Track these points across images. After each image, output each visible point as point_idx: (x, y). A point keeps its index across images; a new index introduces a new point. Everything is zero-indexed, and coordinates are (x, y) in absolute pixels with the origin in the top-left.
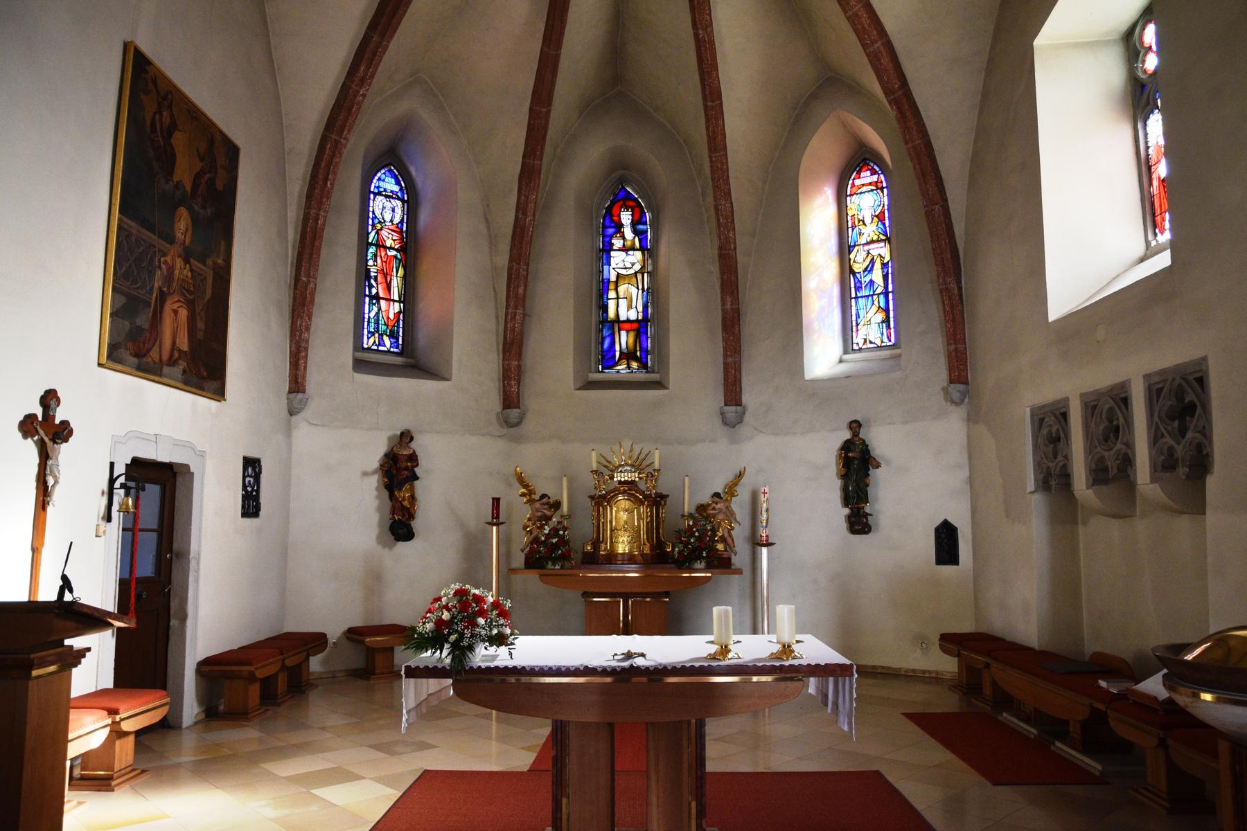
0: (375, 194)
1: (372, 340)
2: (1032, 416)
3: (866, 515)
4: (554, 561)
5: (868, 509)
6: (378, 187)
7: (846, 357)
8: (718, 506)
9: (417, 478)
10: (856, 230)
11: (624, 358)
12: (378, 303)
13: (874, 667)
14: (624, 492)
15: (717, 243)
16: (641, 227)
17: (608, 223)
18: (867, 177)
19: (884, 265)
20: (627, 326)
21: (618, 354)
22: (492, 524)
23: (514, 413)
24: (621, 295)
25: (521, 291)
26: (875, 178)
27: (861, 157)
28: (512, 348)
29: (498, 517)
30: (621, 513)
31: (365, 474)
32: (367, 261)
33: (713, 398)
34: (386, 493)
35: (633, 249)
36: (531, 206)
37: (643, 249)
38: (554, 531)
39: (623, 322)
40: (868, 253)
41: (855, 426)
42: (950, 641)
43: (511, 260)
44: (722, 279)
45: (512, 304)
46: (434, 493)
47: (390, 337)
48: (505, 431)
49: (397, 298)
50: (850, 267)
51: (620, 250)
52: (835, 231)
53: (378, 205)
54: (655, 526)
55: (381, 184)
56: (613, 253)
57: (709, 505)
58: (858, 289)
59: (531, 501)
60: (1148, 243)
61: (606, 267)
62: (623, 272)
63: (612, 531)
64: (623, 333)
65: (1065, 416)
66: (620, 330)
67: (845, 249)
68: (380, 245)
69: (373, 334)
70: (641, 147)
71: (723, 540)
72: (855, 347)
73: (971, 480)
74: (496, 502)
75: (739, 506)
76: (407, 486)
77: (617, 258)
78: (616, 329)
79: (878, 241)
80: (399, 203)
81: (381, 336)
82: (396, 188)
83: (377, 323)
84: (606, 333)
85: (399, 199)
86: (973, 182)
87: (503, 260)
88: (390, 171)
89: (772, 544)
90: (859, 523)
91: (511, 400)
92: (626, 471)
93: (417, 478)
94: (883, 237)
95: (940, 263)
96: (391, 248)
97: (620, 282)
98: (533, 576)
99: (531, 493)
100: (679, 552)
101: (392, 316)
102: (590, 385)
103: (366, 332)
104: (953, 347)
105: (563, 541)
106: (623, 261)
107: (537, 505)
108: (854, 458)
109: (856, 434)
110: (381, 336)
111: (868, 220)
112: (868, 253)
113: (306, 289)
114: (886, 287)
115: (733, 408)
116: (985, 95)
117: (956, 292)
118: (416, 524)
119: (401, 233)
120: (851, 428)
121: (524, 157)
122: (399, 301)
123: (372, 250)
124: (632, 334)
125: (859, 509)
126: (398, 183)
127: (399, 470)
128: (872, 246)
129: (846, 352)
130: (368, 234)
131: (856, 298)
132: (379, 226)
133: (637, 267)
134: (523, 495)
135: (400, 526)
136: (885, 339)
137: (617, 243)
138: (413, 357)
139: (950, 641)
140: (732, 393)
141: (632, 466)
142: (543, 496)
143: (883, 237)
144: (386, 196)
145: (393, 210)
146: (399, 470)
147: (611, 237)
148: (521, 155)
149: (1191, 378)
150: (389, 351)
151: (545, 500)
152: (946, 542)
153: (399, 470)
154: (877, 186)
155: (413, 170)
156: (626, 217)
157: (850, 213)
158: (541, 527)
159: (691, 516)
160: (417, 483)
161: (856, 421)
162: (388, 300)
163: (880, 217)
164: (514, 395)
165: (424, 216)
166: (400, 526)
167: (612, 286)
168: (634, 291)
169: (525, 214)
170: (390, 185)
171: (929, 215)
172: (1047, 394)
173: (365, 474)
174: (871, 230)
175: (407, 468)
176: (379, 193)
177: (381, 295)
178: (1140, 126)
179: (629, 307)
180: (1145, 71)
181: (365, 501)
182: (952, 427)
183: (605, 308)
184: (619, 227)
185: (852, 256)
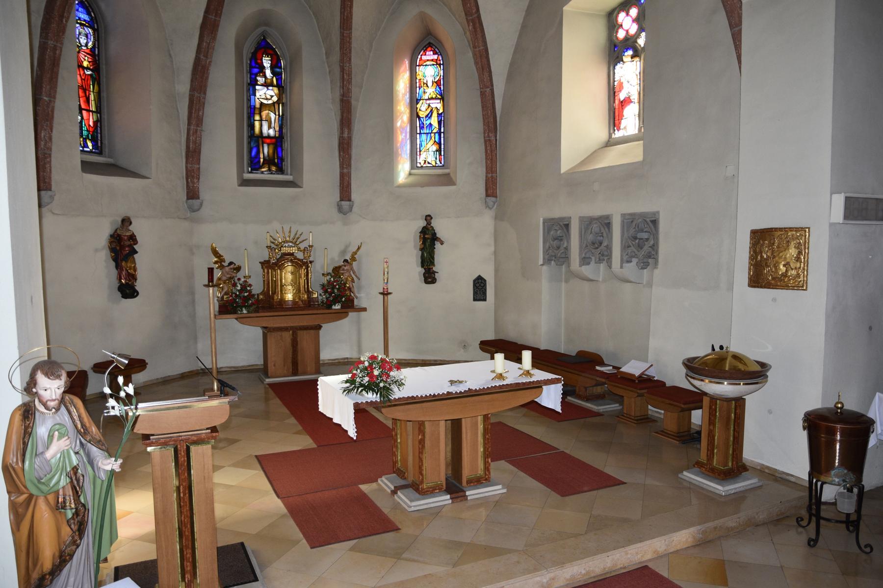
2: (544, 223)
3: (434, 272)
5: (434, 269)
7: (414, 171)
9: (136, 252)
10: (422, 89)
11: (269, 159)
16: (278, 70)
17: (253, 65)
18: (430, 55)
19: (439, 115)
20: (268, 141)
21: (262, 160)
22: (208, 286)
23: (195, 202)
24: (264, 117)
27: (428, 41)
29: (212, 281)
31: (96, 250)
33: (418, 271)
34: (113, 264)
35: (272, 85)
37: (279, 86)
39: (266, 137)
41: (428, 218)
43: (192, 89)
45: (194, 122)
46: (145, 262)
47: (92, 141)
51: (262, 85)
52: (416, 84)
56: (257, 87)
58: (422, 128)
60: (610, 135)
61: (252, 97)
62: (265, 102)
65: (567, 226)
66: (263, 143)
67: (414, 101)
72: (419, 165)
73: (495, 253)
79: (436, 99)
81: (85, 140)
82: (86, 17)
84: (253, 144)
86: (510, 77)
90: (430, 277)
91: (192, 194)
93: (136, 252)
95: (486, 123)
96: (87, 68)
101: (91, 124)
102: (245, 183)
104: (490, 175)
106: (264, 94)
107: (227, 269)
109: (429, 223)
110: (85, 140)
111: (430, 84)
114: (440, 129)
115: (348, 203)
116: (524, 26)
118: (138, 286)
121: (207, 12)
122: (96, 112)
124: (271, 147)
126: (88, 14)
129: (412, 168)
131: (420, 133)
133: (275, 99)
137: (261, 80)
141: (295, 243)
142: (231, 263)
145: (87, 37)
146: (122, 247)
147: (256, 75)
148: (203, 10)
149: (648, 220)
150: (91, 152)
152: (479, 288)
153: (122, 247)
154: (437, 63)
156: (267, 62)
157: (418, 77)
160: (136, 256)
161: (429, 216)
162: (88, 111)
163: (438, 83)
165: (114, 46)
167: (257, 111)
168: (272, 116)
171: (482, 94)
172: (558, 212)
173: (96, 250)
174: (431, 91)
177: (83, 106)
178: (612, 68)
179: (270, 127)
180: (617, 38)
183: (252, 126)
184: (262, 68)
185: (418, 106)
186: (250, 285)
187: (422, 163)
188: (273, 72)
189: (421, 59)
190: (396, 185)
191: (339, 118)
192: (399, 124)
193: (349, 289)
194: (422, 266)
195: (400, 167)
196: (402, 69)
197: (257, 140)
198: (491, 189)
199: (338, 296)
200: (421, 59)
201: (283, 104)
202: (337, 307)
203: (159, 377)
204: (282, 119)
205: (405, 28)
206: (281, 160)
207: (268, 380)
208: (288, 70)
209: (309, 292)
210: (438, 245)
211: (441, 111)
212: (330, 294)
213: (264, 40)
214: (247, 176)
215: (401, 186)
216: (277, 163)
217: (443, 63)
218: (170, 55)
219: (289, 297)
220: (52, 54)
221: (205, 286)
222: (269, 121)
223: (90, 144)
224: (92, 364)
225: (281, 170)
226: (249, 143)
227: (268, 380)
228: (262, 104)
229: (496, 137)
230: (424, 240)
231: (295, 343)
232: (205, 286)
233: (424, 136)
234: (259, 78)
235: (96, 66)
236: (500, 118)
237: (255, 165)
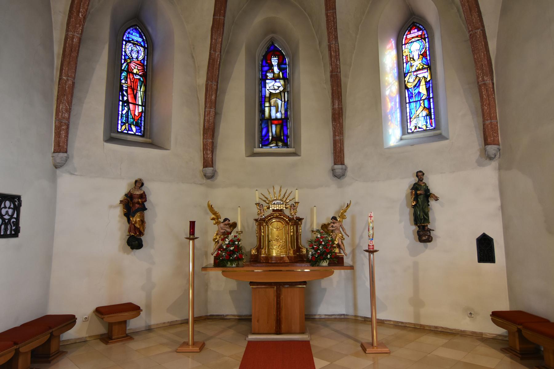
0: (126, 42)
1: (124, 127)
3: (429, 230)
4: (232, 261)
5: (429, 226)
6: (128, 38)
7: (404, 137)
8: (334, 225)
9: (146, 209)
11: (274, 135)
12: (128, 106)
13: (436, 327)
14: (277, 217)
15: (329, 69)
16: (283, 66)
17: (264, 64)
18: (415, 33)
19: (427, 83)
20: (276, 122)
21: (270, 138)
23: (209, 170)
25: (213, 97)
26: (420, 33)
27: (412, 22)
28: (210, 131)
30: (276, 229)
31: (111, 207)
32: (121, 80)
33: (327, 161)
35: (279, 78)
36: (219, 46)
37: (284, 78)
38: (232, 241)
39: (274, 119)
40: (417, 76)
42: (498, 317)
43: (208, 79)
44: (333, 90)
45: (208, 105)
47: (136, 126)
48: (205, 181)
49: (140, 103)
50: (406, 85)
51: (271, 79)
53: (128, 48)
54: (296, 239)
55: (130, 36)
56: (267, 81)
57: (329, 224)
58: (410, 97)
59: (218, 223)
61: (263, 89)
62: (273, 92)
63: (269, 241)
64: (274, 127)
66: (272, 124)
67: (402, 75)
68: (129, 71)
69: (124, 124)
70: (284, 18)
71: (339, 246)
72: (409, 131)
73: (503, 208)
74: (192, 224)
75: (346, 223)
76: (138, 214)
77: (270, 84)
78: (270, 124)
79: (423, 69)
80: (142, 49)
81: (130, 125)
82: (140, 40)
83: (127, 117)
84: (263, 126)
85: (141, 46)
87: (202, 80)
88: (136, 29)
89: (376, 251)
90: (424, 234)
91: (208, 162)
92: (278, 204)
93: (146, 209)
94: (425, 66)
97: (272, 97)
98: (216, 274)
99: (218, 217)
100: (312, 255)
101: (137, 114)
103: (120, 122)
105: (238, 248)
106: (273, 86)
107: (222, 225)
108: (421, 194)
109: (421, 180)
110: (130, 125)
111: (416, 57)
112: (417, 76)
113: (66, 85)
115: (340, 166)
117: (491, 86)
119: (143, 65)
120: (417, 176)
121: (214, 16)
122: (142, 106)
123: (124, 74)
124: (279, 127)
125: (424, 227)
126: (141, 37)
127: (134, 204)
128: (418, 72)
129: (403, 133)
130: (122, 64)
131: (410, 102)
132: (129, 61)
133: (281, 89)
134: (213, 219)
135: (135, 241)
136: (429, 126)
137: (270, 75)
138: (147, 133)
139: (498, 317)
140: (338, 156)
142: (226, 220)
143: (425, 66)
144: (134, 44)
145: (138, 52)
146: (134, 204)
147: (266, 72)
150: (135, 135)
151: (226, 222)
152: (485, 249)
153: (134, 204)
154: (422, 37)
155: (150, 29)
156: (275, 61)
157: (405, 54)
158: (223, 240)
159: (318, 231)
161: (421, 172)
162: (135, 104)
163: (424, 55)
164: (210, 160)
165: (157, 56)
166: (135, 241)
167: (267, 100)
168: (279, 102)
169: (215, 51)
170: (136, 37)
173: (111, 207)
174: (418, 63)
175: (138, 203)
176: (129, 42)
177: (130, 101)
179: (277, 111)
181: (116, 224)
182: (489, 173)
183: (262, 112)
184: (271, 66)
185: (406, 79)
186: (239, 240)
187: (413, 129)
188: (280, 69)
189: (406, 38)
190: (385, 147)
191: (330, 91)
192: (387, 93)
193: (339, 246)
194: (416, 224)
195: (390, 131)
196: (389, 46)
197: (266, 122)
198: (489, 135)
199: (325, 253)
200: (406, 38)
201: (288, 92)
202: (325, 264)
203: (166, 321)
204: (287, 104)
205: (390, 13)
206: (287, 136)
207: (252, 337)
208: (291, 65)
209: (299, 249)
210: (432, 203)
211: (429, 79)
212: (316, 250)
213: (273, 44)
214: (257, 150)
215: (390, 148)
216: (282, 139)
217: (427, 35)
218: (193, 57)
219: (274, 254)
220: (71, 42)
221: (187, 238)
222: (277, 107)
223: (134, 129)
224: (94, 308)
225: (286, 145)
226: (261, 125)
227: (252, 337)
228: (271, 93)
229: (492, 80)
230: (416, 197)
231: (278, 296)
232: (187, 238)
233: (413, 105)
234: (268, 74)
235: (144, 76)
236: (495, 67)
237: (265, 142)
